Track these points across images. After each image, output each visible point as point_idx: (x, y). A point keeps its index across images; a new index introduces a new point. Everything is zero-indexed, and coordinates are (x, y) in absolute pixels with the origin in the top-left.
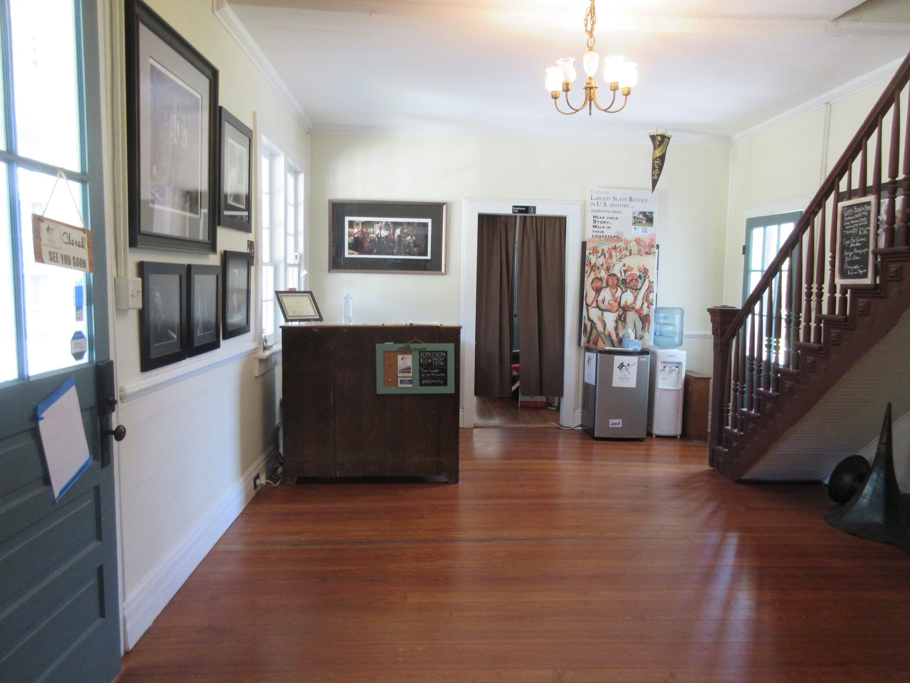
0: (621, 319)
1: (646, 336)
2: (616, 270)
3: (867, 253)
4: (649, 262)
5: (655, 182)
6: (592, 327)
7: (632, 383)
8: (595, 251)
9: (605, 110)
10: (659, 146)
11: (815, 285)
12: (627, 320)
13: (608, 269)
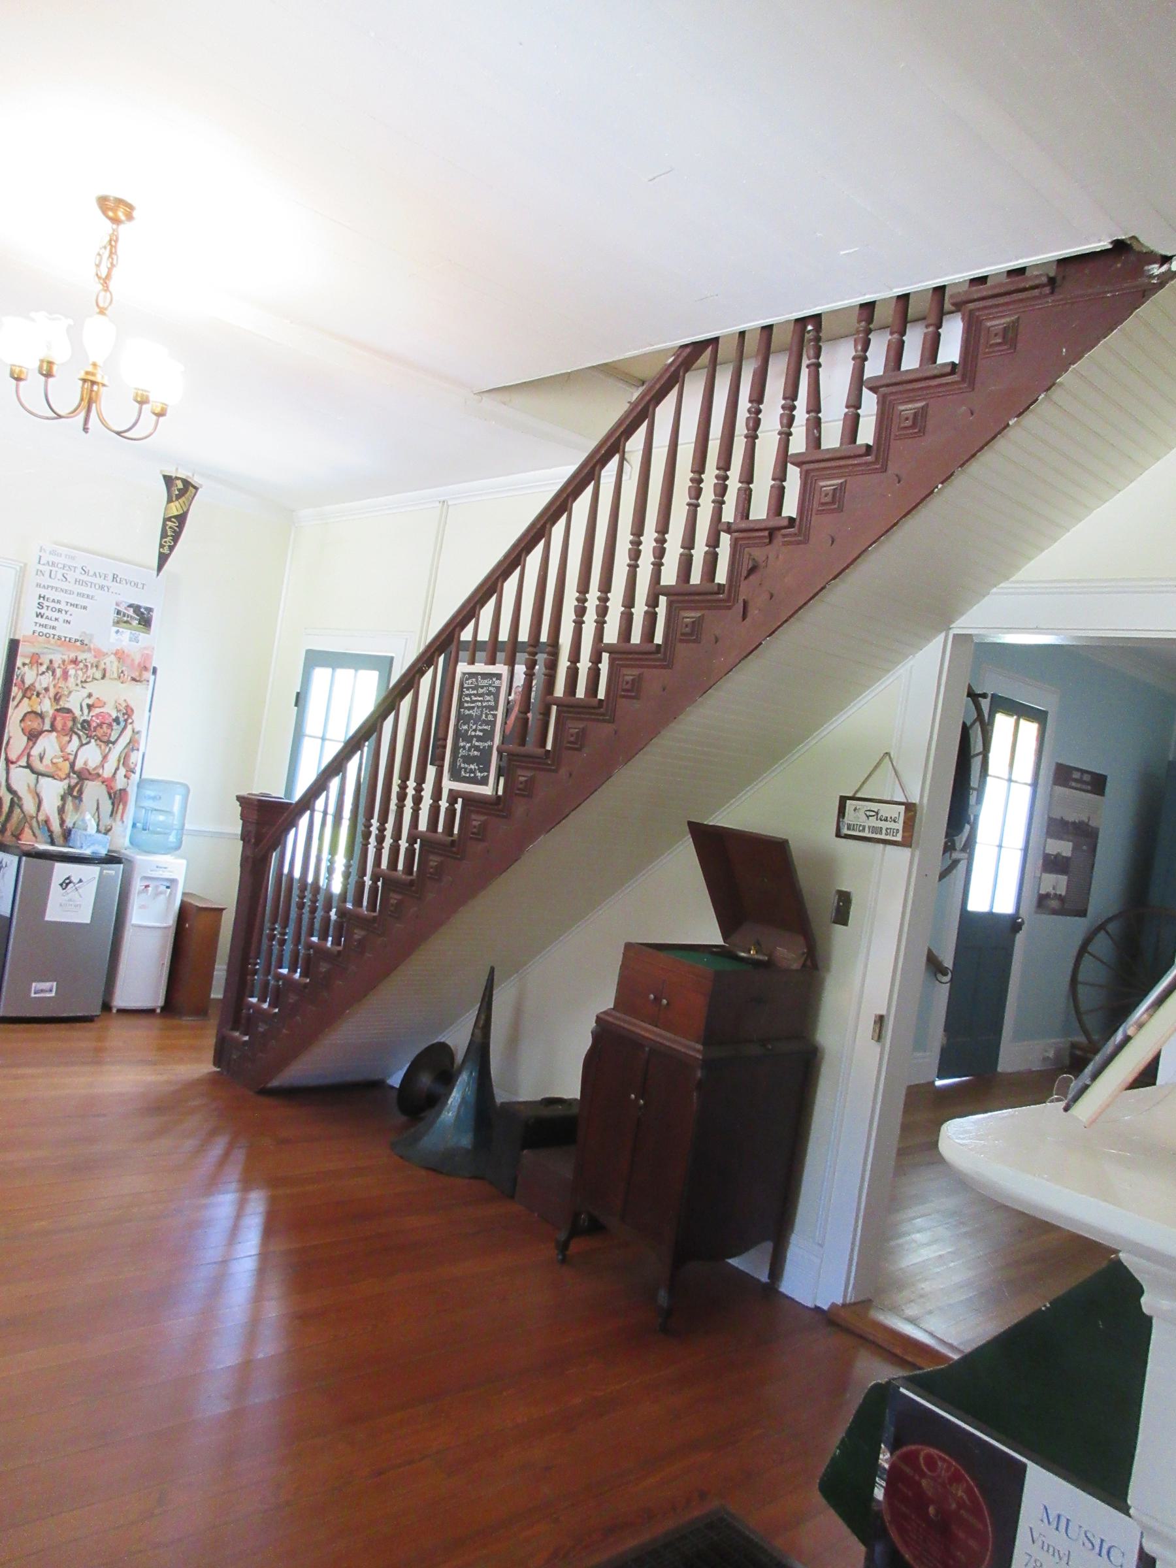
0: (74, 794)
1: (117, 827)
2: (74, 702)
3: (491, 747)
4: (135, 695)
5: (163, 559)
6: (12, 801)
7: (84, 916)
8: (35, 660)
9: (118, 433)
10: (178, 497)
11: (411, 784)
12: (84, 796)
13: (57, 698)
